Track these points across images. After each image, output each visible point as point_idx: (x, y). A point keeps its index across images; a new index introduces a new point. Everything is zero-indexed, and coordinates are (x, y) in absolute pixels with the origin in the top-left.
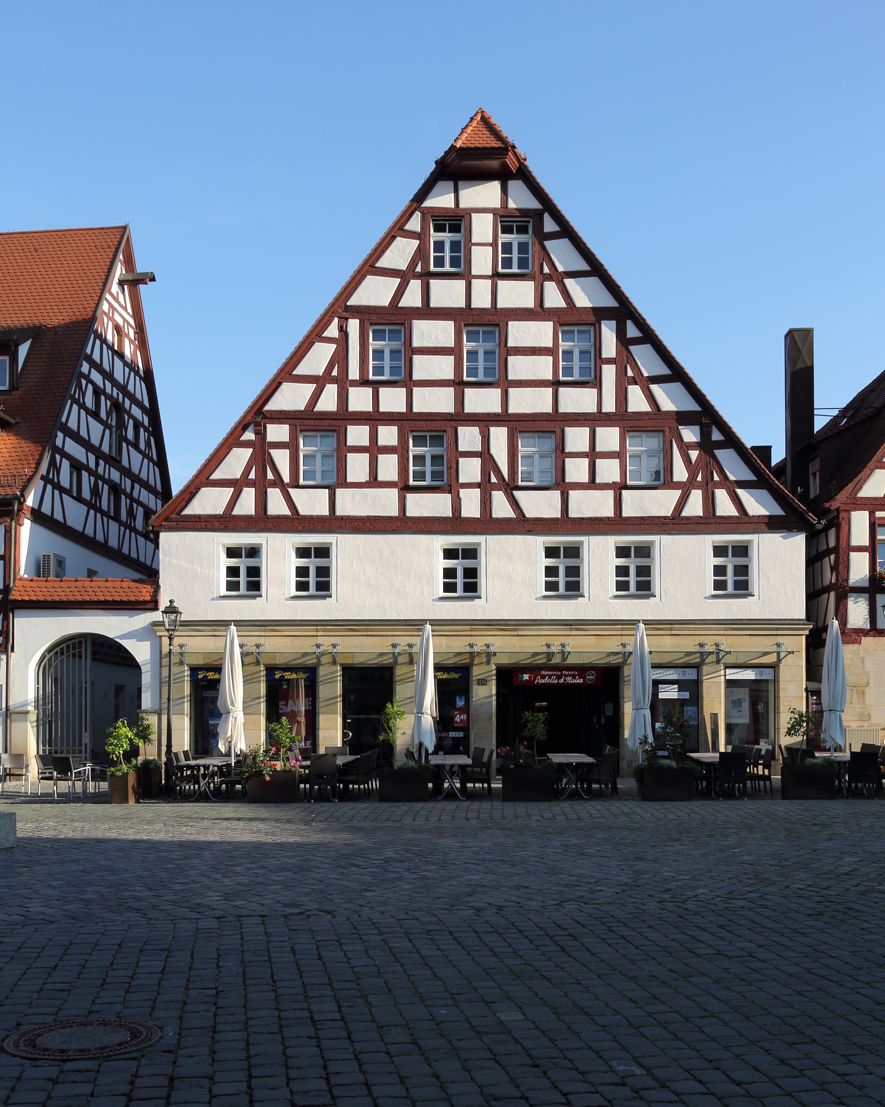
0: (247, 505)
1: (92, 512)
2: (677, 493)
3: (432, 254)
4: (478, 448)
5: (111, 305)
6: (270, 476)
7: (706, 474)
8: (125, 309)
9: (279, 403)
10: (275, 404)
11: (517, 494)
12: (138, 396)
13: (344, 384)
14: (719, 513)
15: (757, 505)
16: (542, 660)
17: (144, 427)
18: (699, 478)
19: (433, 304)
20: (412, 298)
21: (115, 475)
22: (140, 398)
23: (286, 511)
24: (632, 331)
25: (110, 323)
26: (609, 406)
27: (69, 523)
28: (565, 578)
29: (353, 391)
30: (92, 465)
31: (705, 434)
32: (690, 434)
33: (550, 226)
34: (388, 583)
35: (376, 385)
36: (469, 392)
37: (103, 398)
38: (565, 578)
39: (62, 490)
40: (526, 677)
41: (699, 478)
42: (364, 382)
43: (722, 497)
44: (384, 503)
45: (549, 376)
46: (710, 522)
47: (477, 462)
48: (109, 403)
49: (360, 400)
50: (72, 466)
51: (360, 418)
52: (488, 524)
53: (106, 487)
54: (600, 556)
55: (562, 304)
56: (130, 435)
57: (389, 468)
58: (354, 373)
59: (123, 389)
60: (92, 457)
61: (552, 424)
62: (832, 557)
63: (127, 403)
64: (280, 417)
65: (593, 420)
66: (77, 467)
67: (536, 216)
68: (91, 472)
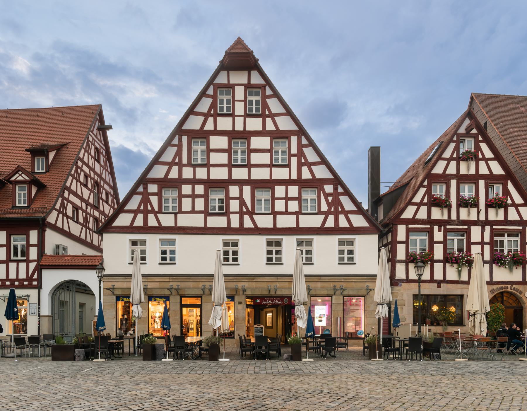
0: (139, 222)
1: (84, 229)
2: (323, 216)
3: (218, 105)
4: (238, 195)
5: (93, 138)
6: (150, 208)
7: (336, 208)
8: (101, 141)
9: (153, 175)
10: (151, 175)
11: (254, 217)
12: (108, 180)
13: (181, 166)
14: (341, 226)
15: (359, 221)
16: (265, 293)
17: (111, 194)
18: (333, 210)
19: (218, 129)
20: (209, 126)
21: (96, 214)
22: (108, 181)
23: (156, 224)
24: (304, 141)
25: (93, 147)
26: (294, 176)
27: (72, 232)
28: (273, 255)
29: (184, 169)
30: (84, 208)
31: (335, 189)
32: (329, 189)
33: (269, 92)
34: (198, 255)
35: (195, 166)
36: (234, 170)
37: (89, 179)
38: (273, 255)
39: (68, 217)
40: (258, 301)
41: (333, 210)
42: (189, 164)
43: (342, 218)
44: (197, 221)
45: (268, 162)
46: (336, 230)
47: (238, 202)
48: (92, 181)
49: (187, 173)
50: (73, 207)
51: (187, 182)
52: (242, 231)
53: (91, 218)
54: (289, 243)
55: (274, 129)
56: (104, 196)
57: (200, 204)
58: (185, 161)
59: (100, 176)
60: (84, 205)
61: (269, 184)
62: (390, 246)
63: (102, 183)
64: (154, 181)
65: (287, 183)
66: (76, 208)
67: (262, 87)
68: (83, 211)
